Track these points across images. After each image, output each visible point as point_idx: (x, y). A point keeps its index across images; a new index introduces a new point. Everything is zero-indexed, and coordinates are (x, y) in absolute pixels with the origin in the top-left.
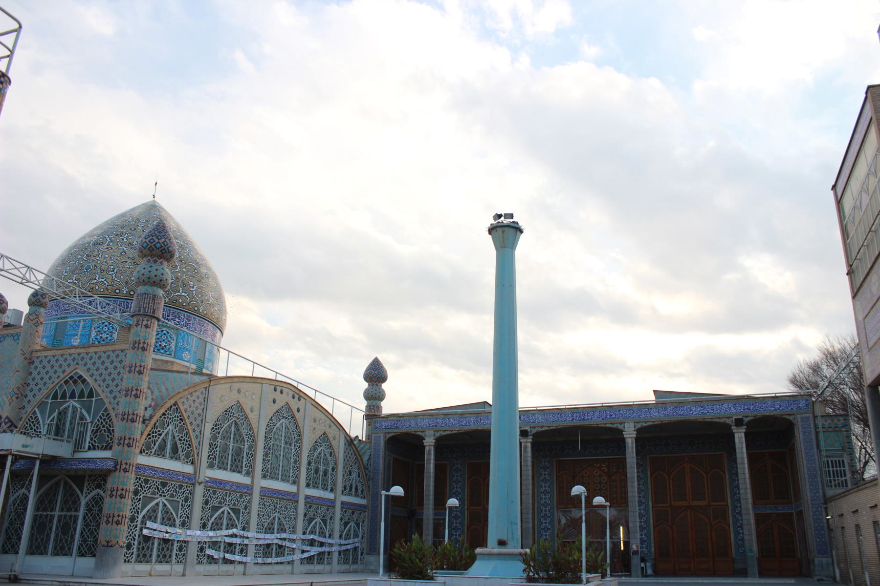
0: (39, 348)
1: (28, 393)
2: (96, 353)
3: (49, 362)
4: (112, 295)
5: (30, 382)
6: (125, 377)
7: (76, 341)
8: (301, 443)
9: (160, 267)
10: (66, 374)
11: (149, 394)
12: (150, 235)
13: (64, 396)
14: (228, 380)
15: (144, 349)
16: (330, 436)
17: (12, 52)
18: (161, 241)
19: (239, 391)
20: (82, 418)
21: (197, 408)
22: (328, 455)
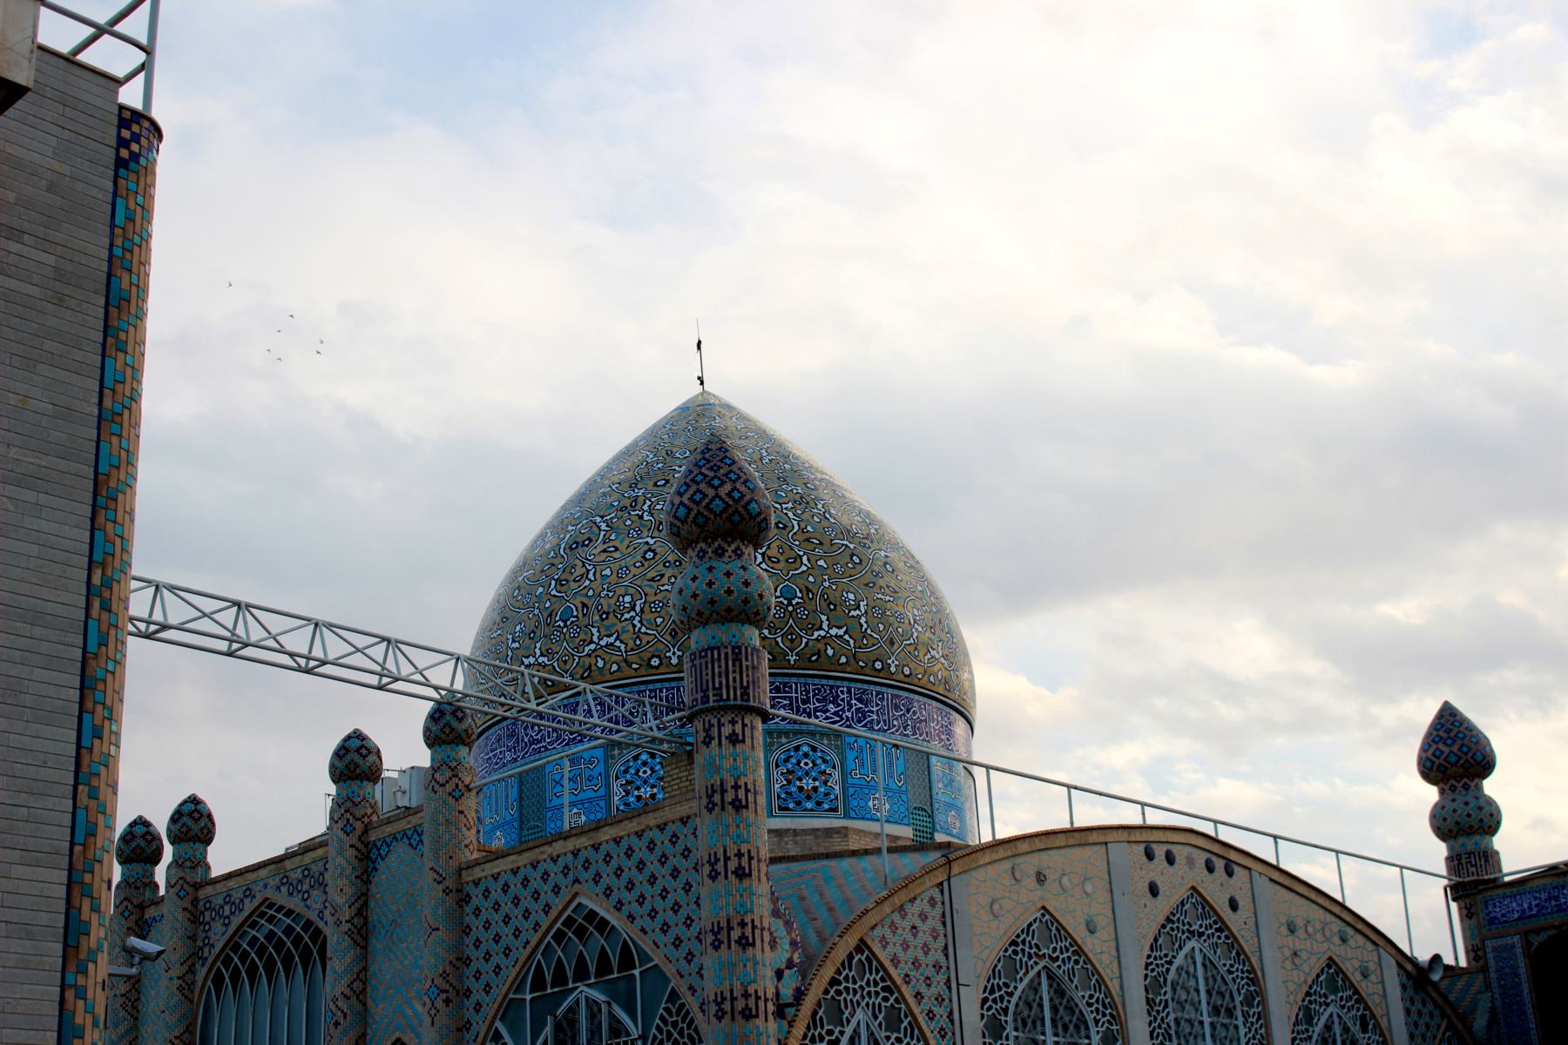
0: (476, 855)
1: (471, 983)
2: (617, 841)
3: (506, 888)
4: (642, 676)
5: (471, 951)
6: (704, 892)
7: (570, 818)
8: (1263, 1002)
9: (1469, 798)
10: (553, 913)
11: (781, 931)
12: (690, 481)
13: (560, 978)
14: (1001, 853)
15: (738, 806)
16: (1351, 968)
17: (148, 50)
18: (723, 492)
19: (1041, 878)
20: (617, 1029)
21: (926, 949)
22: (1355, 1029)
